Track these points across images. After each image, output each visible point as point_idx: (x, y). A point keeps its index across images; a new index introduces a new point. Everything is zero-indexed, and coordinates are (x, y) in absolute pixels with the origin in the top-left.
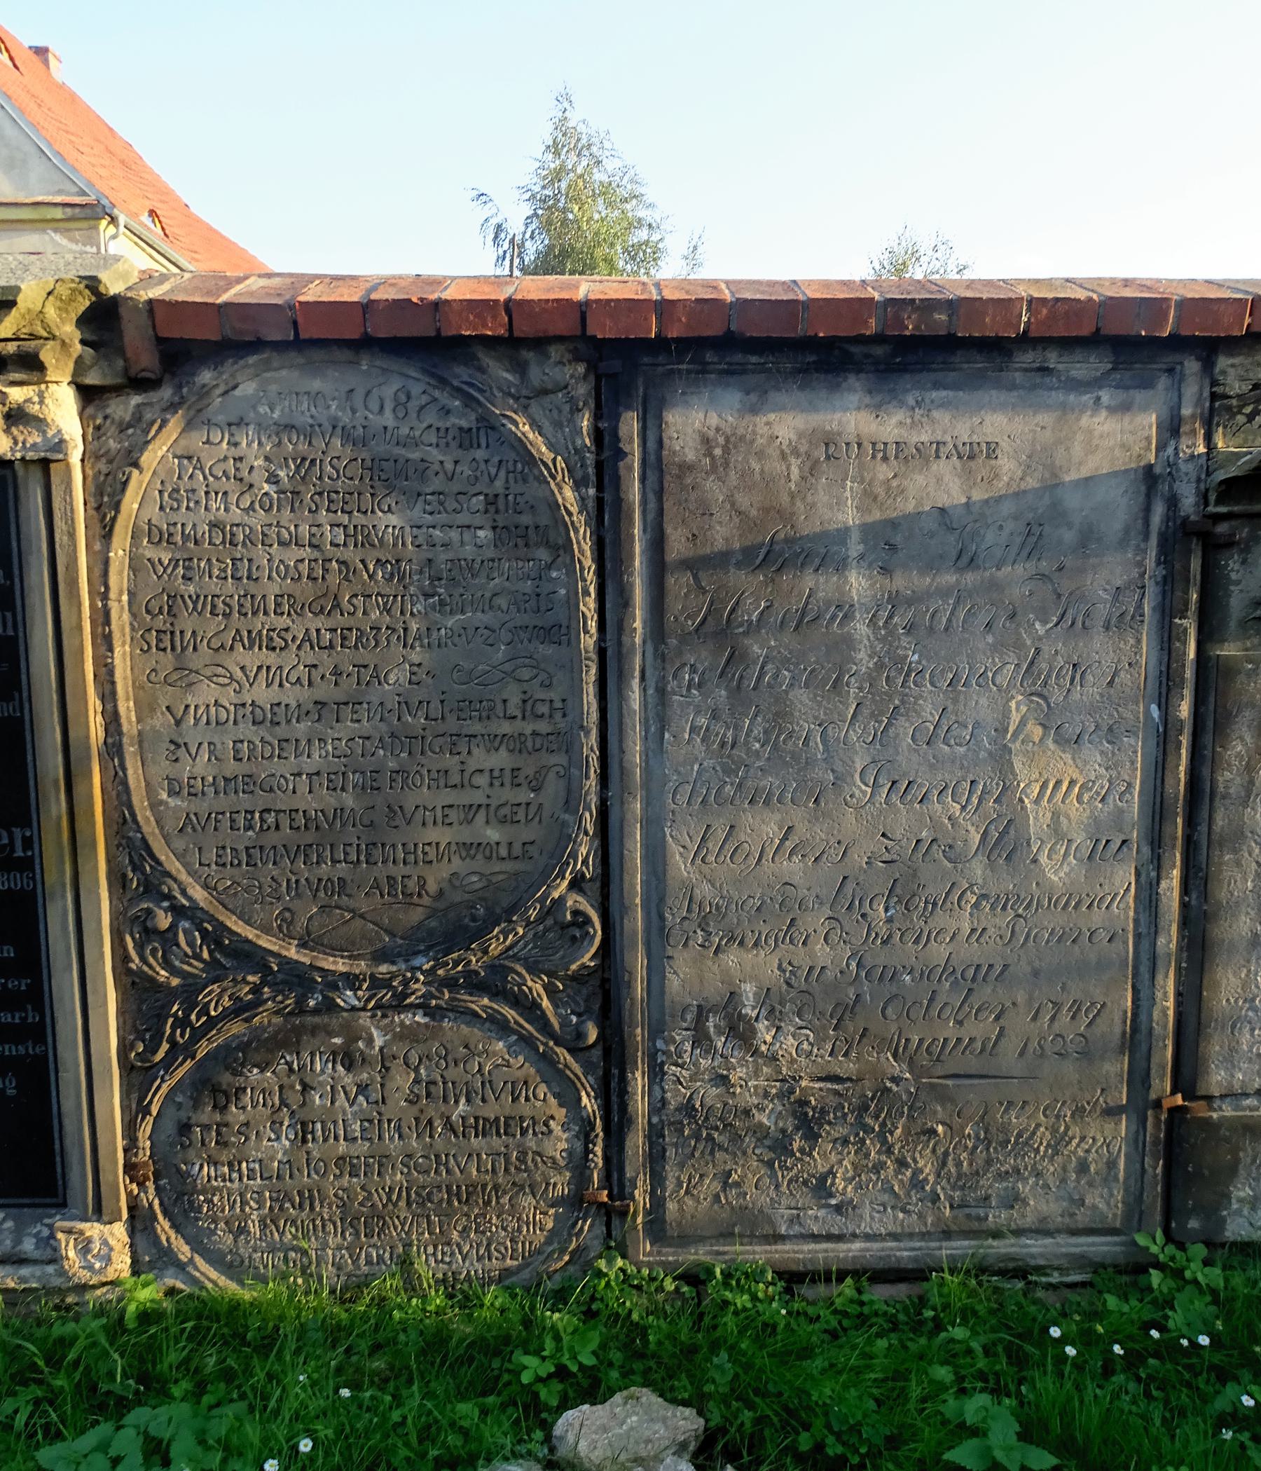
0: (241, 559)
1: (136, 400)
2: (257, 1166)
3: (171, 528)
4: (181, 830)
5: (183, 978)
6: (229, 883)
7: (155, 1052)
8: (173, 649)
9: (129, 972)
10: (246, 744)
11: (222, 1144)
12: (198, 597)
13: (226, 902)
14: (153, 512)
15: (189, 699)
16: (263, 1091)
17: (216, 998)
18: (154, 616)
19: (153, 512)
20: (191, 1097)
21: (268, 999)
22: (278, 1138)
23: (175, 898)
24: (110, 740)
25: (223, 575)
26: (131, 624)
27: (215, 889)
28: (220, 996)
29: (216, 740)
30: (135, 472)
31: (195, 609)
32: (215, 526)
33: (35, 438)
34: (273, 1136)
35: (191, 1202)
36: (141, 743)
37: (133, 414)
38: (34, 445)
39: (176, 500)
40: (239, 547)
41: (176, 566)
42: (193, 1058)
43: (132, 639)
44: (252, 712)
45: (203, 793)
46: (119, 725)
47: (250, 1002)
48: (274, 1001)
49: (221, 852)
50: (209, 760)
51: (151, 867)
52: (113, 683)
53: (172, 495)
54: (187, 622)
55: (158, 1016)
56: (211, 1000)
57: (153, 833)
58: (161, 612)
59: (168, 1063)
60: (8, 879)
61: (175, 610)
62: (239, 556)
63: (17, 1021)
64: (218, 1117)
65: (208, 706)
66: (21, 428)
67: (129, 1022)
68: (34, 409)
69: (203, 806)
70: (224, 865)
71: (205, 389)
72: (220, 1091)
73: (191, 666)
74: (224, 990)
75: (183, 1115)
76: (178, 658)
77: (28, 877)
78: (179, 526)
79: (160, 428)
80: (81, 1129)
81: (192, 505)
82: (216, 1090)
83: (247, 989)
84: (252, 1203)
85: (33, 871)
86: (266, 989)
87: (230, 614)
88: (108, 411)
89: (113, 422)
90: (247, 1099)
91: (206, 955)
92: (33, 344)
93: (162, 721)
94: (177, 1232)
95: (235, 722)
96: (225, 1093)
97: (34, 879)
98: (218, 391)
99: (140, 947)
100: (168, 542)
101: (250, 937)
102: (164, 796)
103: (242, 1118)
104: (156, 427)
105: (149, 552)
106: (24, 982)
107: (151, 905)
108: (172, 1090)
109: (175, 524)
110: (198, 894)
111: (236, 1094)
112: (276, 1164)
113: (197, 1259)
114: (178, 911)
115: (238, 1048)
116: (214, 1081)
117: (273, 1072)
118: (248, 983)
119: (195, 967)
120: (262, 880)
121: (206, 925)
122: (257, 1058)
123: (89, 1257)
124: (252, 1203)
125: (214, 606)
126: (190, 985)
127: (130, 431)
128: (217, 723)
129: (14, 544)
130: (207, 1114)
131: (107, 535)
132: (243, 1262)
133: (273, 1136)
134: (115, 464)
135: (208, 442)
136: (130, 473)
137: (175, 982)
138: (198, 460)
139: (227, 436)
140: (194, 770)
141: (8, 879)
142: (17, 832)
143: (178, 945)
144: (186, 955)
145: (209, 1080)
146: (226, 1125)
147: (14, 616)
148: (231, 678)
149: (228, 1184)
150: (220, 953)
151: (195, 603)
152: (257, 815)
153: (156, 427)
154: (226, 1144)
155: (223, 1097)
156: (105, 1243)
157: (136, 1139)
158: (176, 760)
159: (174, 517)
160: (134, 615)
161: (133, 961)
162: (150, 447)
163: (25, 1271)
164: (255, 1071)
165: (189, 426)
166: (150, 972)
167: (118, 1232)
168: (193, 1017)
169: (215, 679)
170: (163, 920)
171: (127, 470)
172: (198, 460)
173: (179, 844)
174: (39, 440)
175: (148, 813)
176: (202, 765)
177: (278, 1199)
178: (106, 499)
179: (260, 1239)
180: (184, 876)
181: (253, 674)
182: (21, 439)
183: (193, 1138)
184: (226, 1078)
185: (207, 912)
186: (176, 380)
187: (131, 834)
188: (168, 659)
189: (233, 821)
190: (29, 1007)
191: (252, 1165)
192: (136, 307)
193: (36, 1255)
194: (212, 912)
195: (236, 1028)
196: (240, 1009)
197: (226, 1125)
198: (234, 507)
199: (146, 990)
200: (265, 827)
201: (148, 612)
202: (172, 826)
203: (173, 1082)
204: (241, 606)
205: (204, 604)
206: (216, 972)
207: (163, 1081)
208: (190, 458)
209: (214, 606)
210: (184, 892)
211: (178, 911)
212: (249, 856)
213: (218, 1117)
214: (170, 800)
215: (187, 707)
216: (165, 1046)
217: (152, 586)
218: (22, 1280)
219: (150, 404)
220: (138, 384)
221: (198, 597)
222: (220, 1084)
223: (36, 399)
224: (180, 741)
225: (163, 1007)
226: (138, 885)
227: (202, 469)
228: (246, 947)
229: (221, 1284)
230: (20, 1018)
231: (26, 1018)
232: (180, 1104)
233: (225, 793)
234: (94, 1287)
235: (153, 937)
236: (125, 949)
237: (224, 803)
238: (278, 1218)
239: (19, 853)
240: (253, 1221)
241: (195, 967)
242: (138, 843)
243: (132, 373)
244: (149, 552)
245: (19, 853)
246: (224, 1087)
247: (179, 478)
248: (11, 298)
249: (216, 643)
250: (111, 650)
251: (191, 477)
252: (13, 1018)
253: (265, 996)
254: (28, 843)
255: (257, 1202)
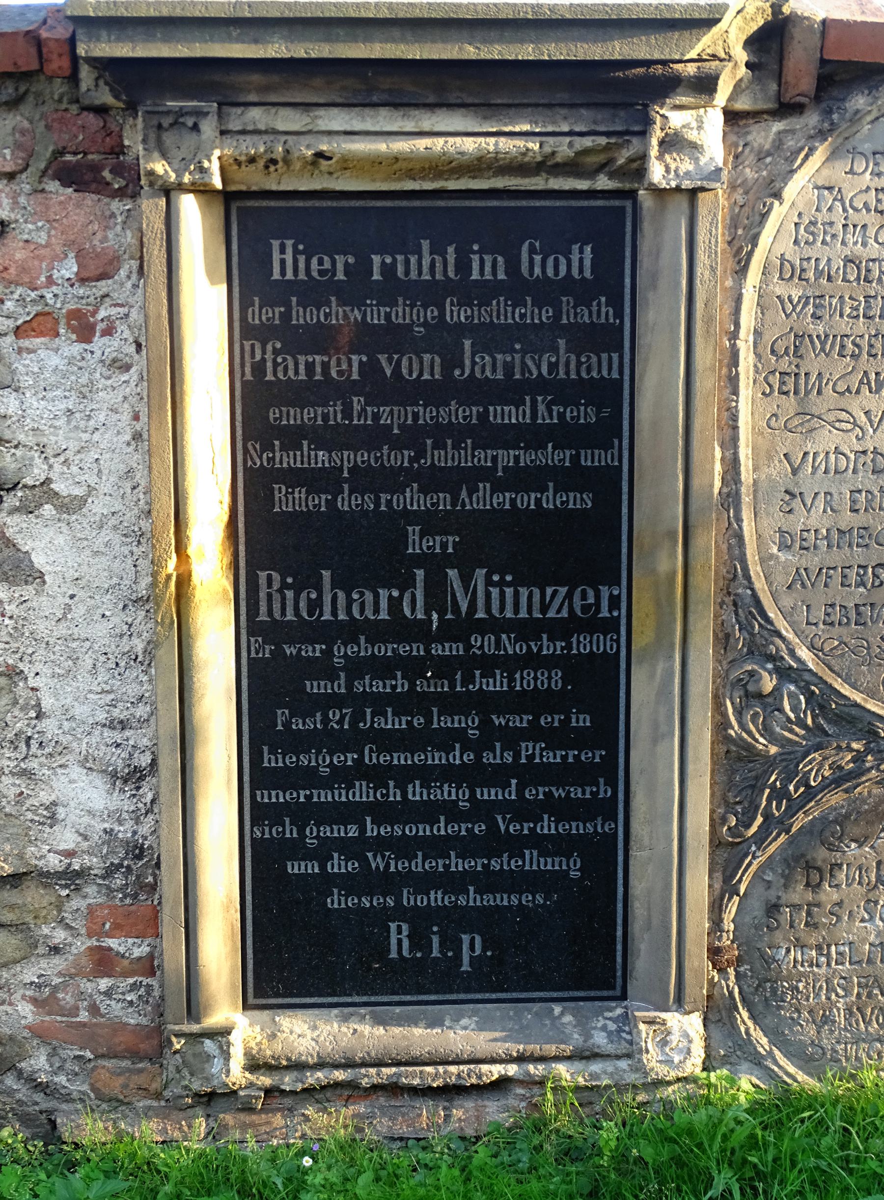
0: (875, 297)
1: (777, 126)
2: (847, 950)
3: (805, 263)
4: (789, 587)
5: (782, 746)
6: (836, 643)
7: (748, 826)
8: (796, 393)
9: (728, 739)
10: (864, 494)
11: (812, 925)
12: (827, 336)
13: (833, 662)
14: (786, 247)
15: (810, 447)
16: (860, 868)
17: (816, 767)
18: (779, 357)
19: (786, 247)
20: (782, 875)
21: (872, 768)
22: (872, 918)
23: (782, 658)
24: (725, 490)
25: (855, 314)
26: (755, 366)
27: (822, 650)
28: (821, 765)
29: (833, 491)
30: (777, 203)
31: (823, 349)
32: (851, 261)
33: (687, 166)
34: (866, 916)
35: (774, 991)
36: (755, 492)
37: (774, 141)
38: (687, 173)
39: (812, 233)
40: (874, 284)
41: (806, 304)
42: (787, 832)
43: (755, 382)
44: (872, 461)
45: (815, 547)
46: (738, 474)
47: (850, 772)
48: (878, 770)
49: (830, 610)
50: (825, 511)
51: (760, 625)
52: (735, 428)
53: (808, 229)
54: (813, 364)
55: (753, 787)
56: (812, 770)
57: (763, 589)
58: (787, 353)
59: (761, 839)
60: (591, 642)
61: (802, 351)
62: (873, 294)
63: (588, 796)
64: (810, 896)
65: (827, 453)
66: (675, 155)
67: (718, 794)
68: (692, 135)
69: (813, 561)
70: (832, 624)
71: (858, 116)
72: (815, 868)
73: (815, 411)
74: (825, 759)
75: (772, 895)
76: (800, 402)
77: (611, 639)
78: (813, 261)
79: (807, 157)
80: (668, 910)
81: (828, 238)
82: (809, 866)
83: (849, 757)
84: (839, 990)
85: (618, 633)
86: (869, 758)
87: (859, 356)
88: (750, 138)
89: (751, 151)
90: (842, 876)
91: (809, 721)
92: (715, 64)
93: (778, 470)
94: (756, 1023)
95: (855, 471)
96: (819, 870)
97: (618, 641)
98: (869, 118)
99: (739, 713)
100: (800, 279)
101: (859, 701)
102: (775, 550)
103: (835, 897)
104: (802, 155)
105: (780, 289)
106: (598, 753)
107: (756, 667)
108: (762, 868)
109: (809, 259)
110: (804, 653)
111: (831, 870)
112: (867, 947)
113: (777, 1053)
114: (784, 673)
115: (836, 821)
116: (809, 857)
117: (872, 847)
118: (852, 750)
119: (797, 735)
120: (871, 639)
121: (813, 688)
122: (856, 831)
123: (667, 1049)
124: (839, 990)
125: (843, 346)
126: (789, 753)
127: (768, 160)
128: (836, 472)
129: (628, 281)
130: (799, 894)
131: (742, 271)
132: (824, 1054)
133: (866, 916)
134: (751, 195)
135: (851, 172)
136: (772, 204)
137: (773, 750)
138: (840, 190)
139: (871, 165)
140: (808, 522)
141: (591, 642)
142: (605, 591)
143: (781, 710)
144: (789, 720)
145: (803, 855)
146: (818, 905)
147: (621, 358)
148: (855, 424)
149: (815, 968)
150: (825, 718)
151: (823, 344)
152: (870, 570)
153: (802, 155)
154: (816, 926)
155: (817, 875)
156: (686, 1035)
157: (721, 920)
158: (790, 512)
159: (808, 252)
160: (758, 355)
161: (733, 729)
162: (796, 176)
163: (596, 1067)
164: (853, 845)
165: (833, 155)
166: (750, 740)
167: (693, 1023)
168: (791, 788)
169: (837, 425)
170: (768, 683)
171: (769, 201)
172: (840, 190)
173: (787, 602)
174: (691, 167)
175: (759, 568)
176: (817, 518)
177: (867, 986)
178: (740, 232)
179: (846, 1029)
180: (790, 635)
181: (877, 420)
182: (673, 166)
183: (782, 919)
184: (821, 854)
185: (815, 674)
186: (824, 105)
187: (740, 591)
188: (790, 404)
189: (844, 576)
190: (602, 780)
191: (842, 948)
192: (811, 27)
193: (610, 1049)
194: (820, 674)
195: (835, 799)
196: (841, 779)
197: (818, 905)
198: (872, 241)
199: (740, 759)
200: (877, 584)
201: (773, 352)
202: (781, 580)
203: (762, 859)
204: (871, 346)
205: (834, 344)
206: (818, 738)
207: (754, 857)
208: (830, 188)
209: (843, 346)
210: (792, 653)
211: (784, 673)
212: (858, 614)
213: (810, 896)
214: (780, 554)
215: (806, 454)
216: (759, 820)
217: (779, 326)
218: (594, 1076)
219: (792, 132)
220: (786, 109)
221: (827, 336)
222: (814, 859)
223: (694, 124)
224: (796, 491)
225: (757, 778)
226: (743, 645)
227: (842, 200)
228: (854, 711)
229: (800, 1079)
230: (592, 793)
231: (598, 792)
232: (769, 882)
233: (838, 547)
234: (669, 1083)
235: (753, 702)
236: (725, 715)
237: (837, 557)
238: (866, 1005)
239: (605, 613)
240: (838, 1010)
241: (797, 735)
242: (748, 600)
243: (787, 98)
244: (780, 289)
245: (605, 613)
246: (819, 863)
247: (817, 210)
248: (717, 16)
249: (841, 388)
250: (736, 392)
251: (830, 209)
252: (584, 793)
253: (868, 765)
254: (614, 603)
255: (844, 989)
